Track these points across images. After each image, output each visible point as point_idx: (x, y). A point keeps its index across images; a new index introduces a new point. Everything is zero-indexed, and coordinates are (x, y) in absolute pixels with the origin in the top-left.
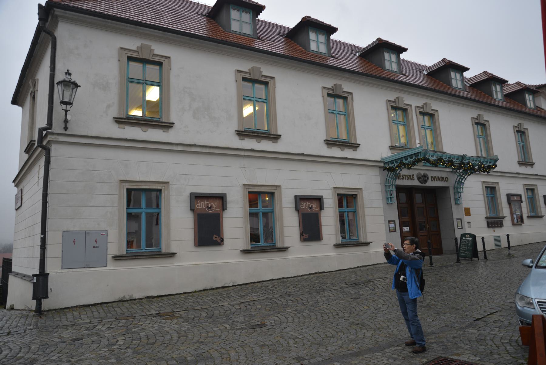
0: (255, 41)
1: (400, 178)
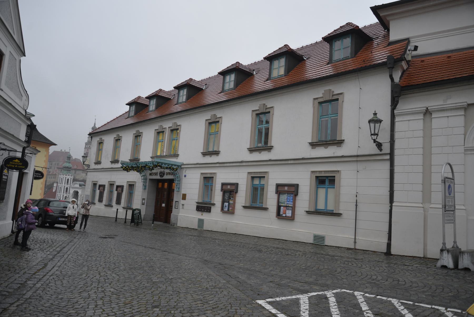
0: (390, 53)
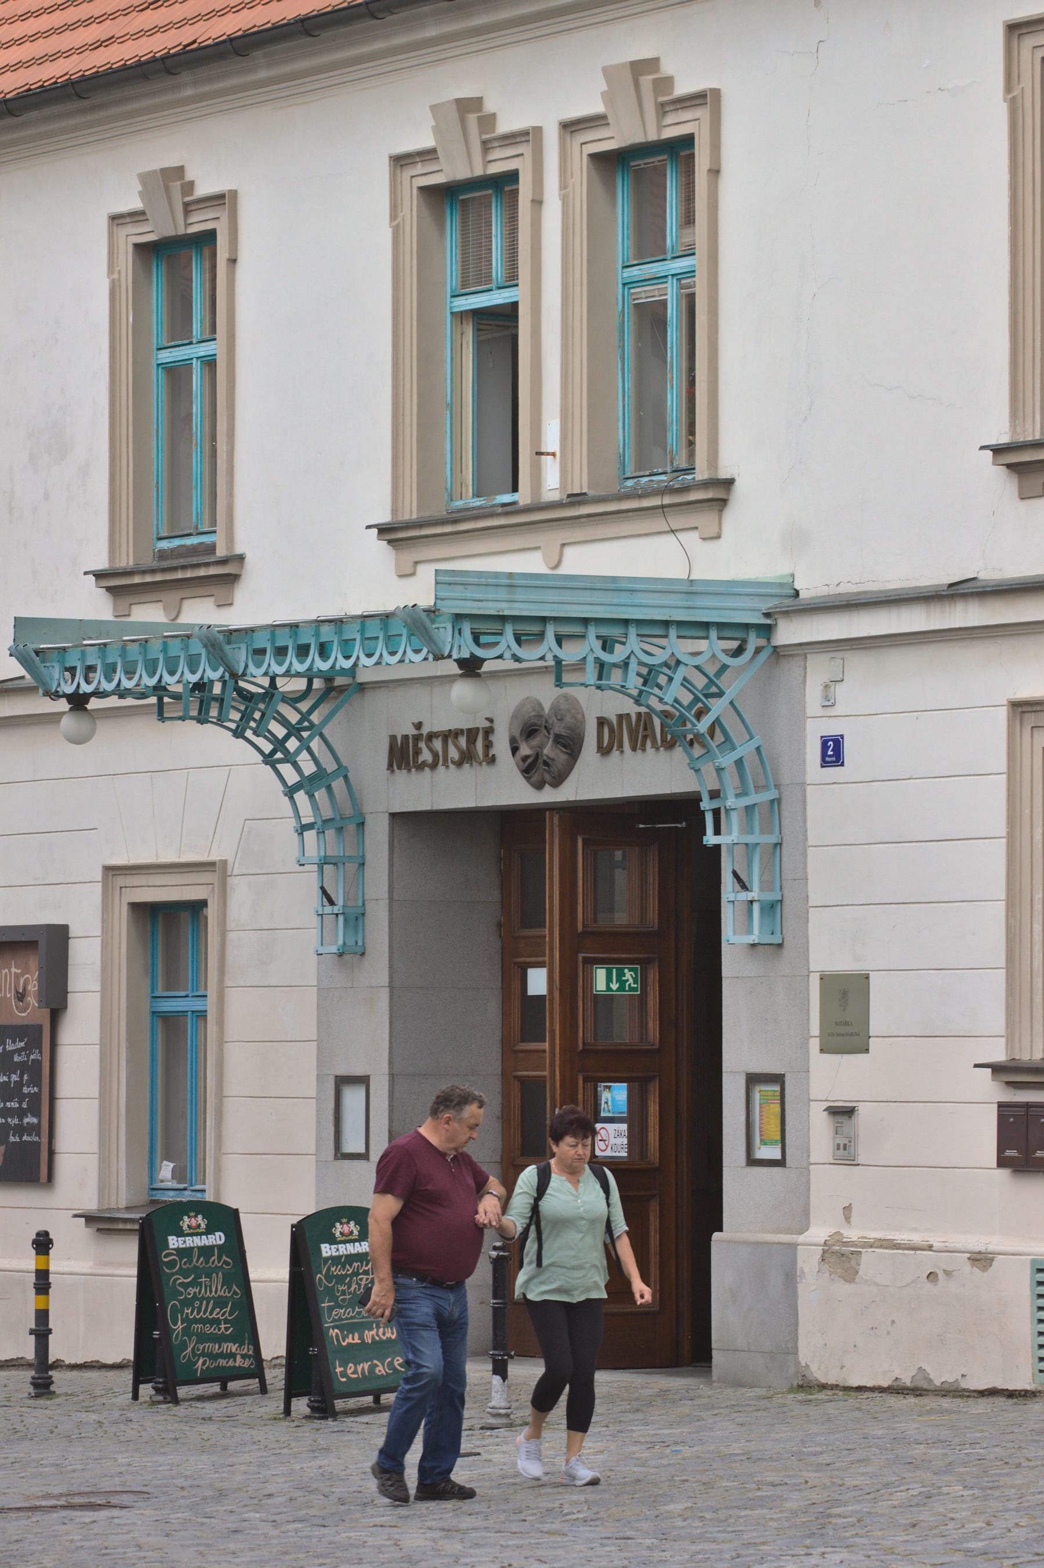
1: (415, 761)
